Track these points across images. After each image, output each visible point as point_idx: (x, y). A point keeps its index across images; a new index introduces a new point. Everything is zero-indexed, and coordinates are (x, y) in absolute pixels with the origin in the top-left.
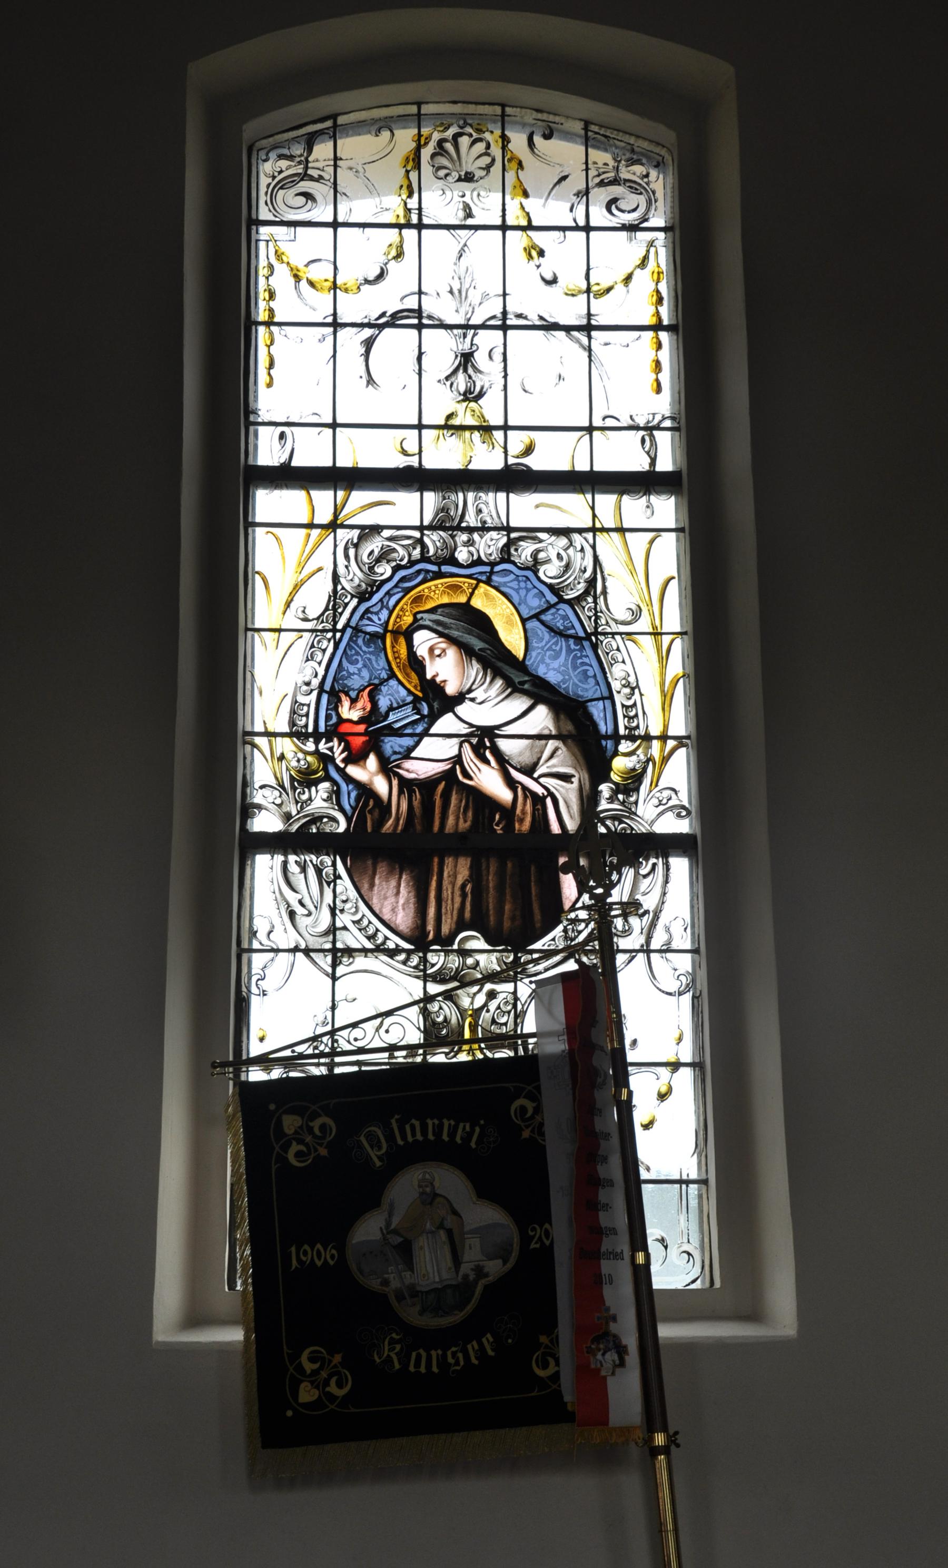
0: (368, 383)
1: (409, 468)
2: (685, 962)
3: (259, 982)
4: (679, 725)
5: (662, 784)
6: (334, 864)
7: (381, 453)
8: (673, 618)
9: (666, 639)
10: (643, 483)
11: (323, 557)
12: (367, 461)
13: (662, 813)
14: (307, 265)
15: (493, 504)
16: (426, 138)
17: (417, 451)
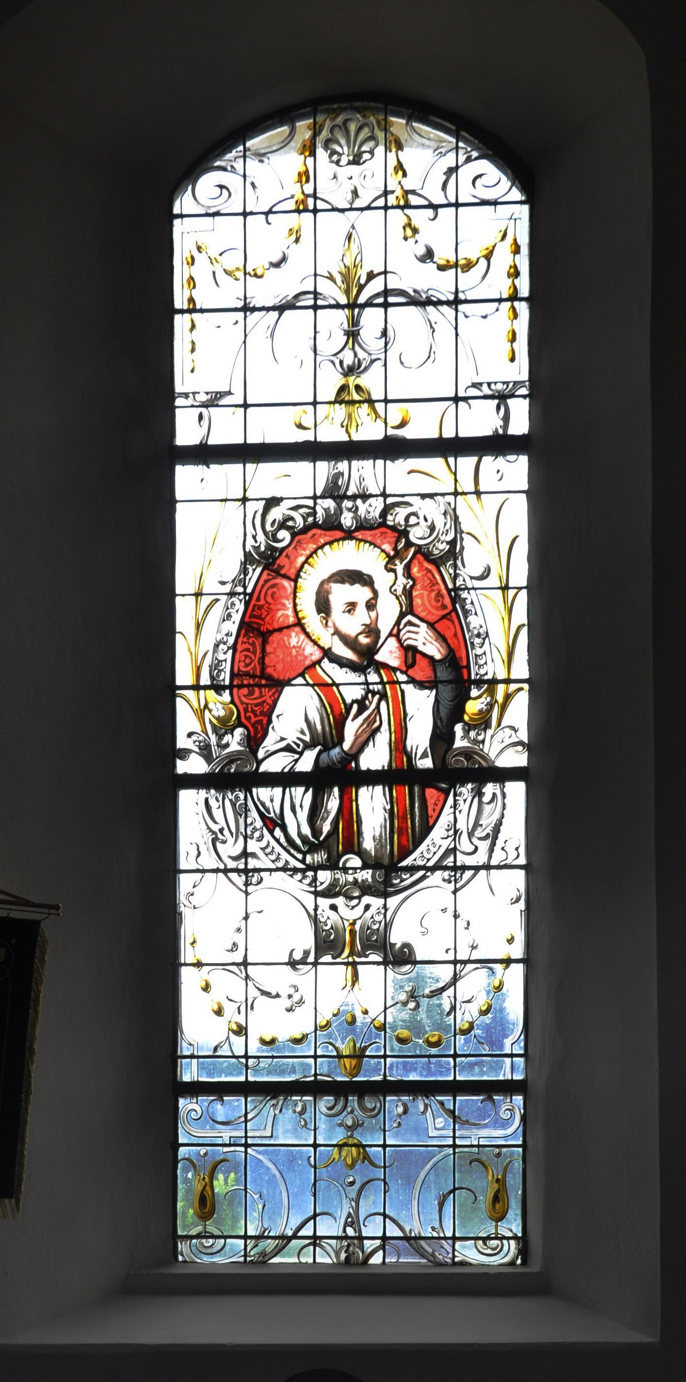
2: (518, 879)
4: (521, 669)
5: (503, 724)
7: (277, 428)
8: (520, 574)
9: (511, 593)
10: (499, 444)
14: (221, 255)
15: (365, 473)
16: (321, 126)
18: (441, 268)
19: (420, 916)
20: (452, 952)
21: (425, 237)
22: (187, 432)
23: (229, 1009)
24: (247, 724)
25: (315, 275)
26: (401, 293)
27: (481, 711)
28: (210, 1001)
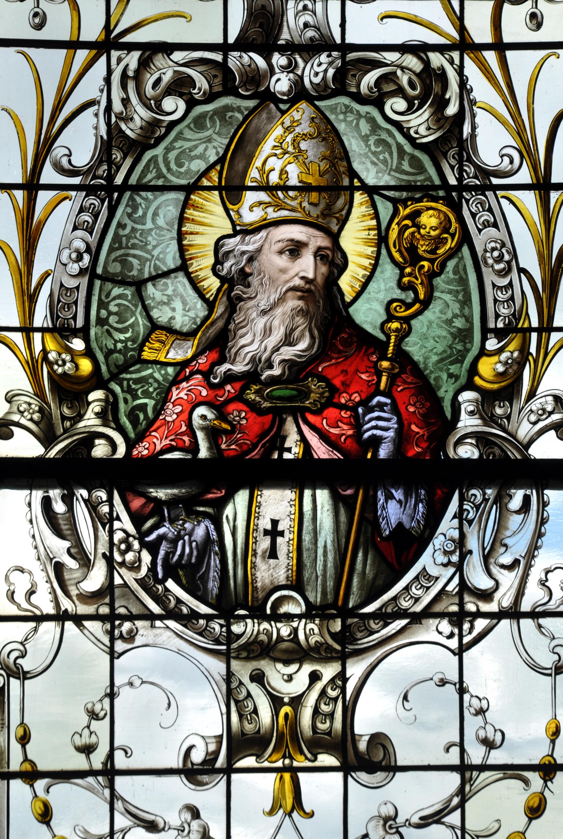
3: (19, 661)
11: (91, 87)
20: (455, 751)
24: (417, 153)
27: (501, 375)
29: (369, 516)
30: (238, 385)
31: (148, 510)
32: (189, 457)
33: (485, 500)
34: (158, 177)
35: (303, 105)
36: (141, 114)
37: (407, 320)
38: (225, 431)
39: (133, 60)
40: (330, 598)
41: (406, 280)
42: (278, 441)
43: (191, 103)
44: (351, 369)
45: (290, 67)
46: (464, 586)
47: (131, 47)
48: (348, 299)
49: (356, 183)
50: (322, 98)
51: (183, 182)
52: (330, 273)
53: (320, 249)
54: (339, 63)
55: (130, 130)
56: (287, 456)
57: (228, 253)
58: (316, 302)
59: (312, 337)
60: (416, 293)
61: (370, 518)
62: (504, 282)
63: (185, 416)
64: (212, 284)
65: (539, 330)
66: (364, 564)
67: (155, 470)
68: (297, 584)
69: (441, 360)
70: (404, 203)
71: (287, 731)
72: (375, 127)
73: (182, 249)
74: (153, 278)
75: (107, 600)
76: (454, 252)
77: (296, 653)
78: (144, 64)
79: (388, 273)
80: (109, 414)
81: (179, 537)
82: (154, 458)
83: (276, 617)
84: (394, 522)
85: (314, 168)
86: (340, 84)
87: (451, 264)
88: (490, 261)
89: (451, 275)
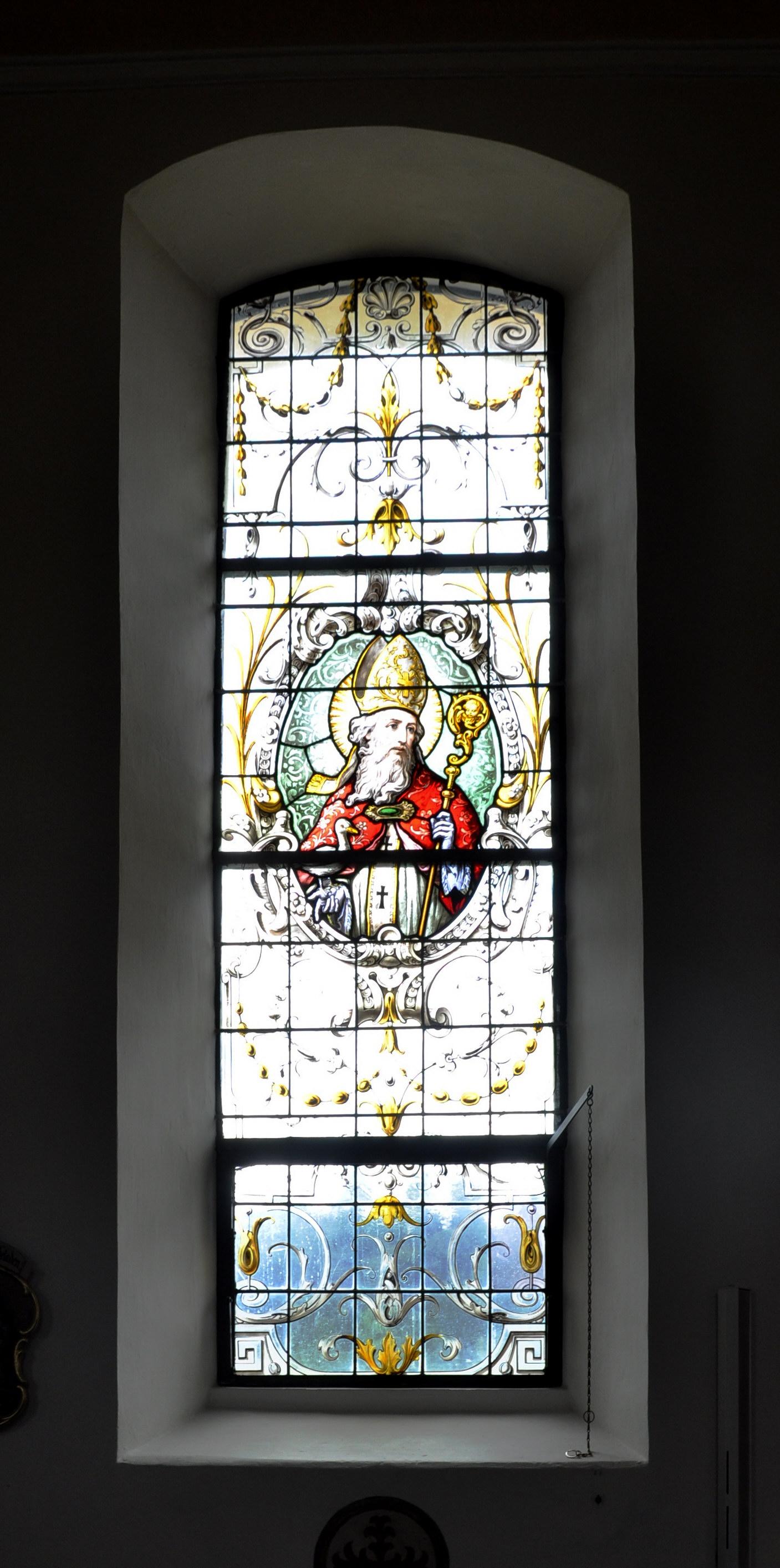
0: (318, 488)
1: (348, 558)
6: (288, 876)
10: (356, 1132)
11: (281, 631)
12: (316, 553)
13: (535, 832)
17: (354, 541)
18: (473, 407)
19: (455, 980)
21: (458, 382)
22: (236, 545)
23: (273, 1074)
24: (464, 666)
25: (356, 412)
26: (438, 428)
28: (255, 1066)
29: (437, 883)
30: (363, 806)
31: (310, 881)
32: (334, 849)
33: (504, 873)
34: (318, 682)
35: (399, 638)
36: (308, 646)
37: (459, 766)
38: (355, 834)
39: (303, 613)
40: (415, 931)
41: (458, 742)
42: (385, 840)
43: (337, 638)
44: (427, 796)
45: (392, 615)
46: (491, 924)
47: (302, 606)
48: (425, 754)
49: (430, 684)
50: (410, 633)
51: (331, 686)
52: (415, 738)
53: (409, 724)
54: (419, 612)
55: (303, 655)
56: (390, 848)
57: (356, 728)
58: (407, 756)
59: (405, 777)
60: (464, 749)
61: (438, 885)
62: (513, 743)
63: (332, 825)
64: (347, 747)
65: (534, 771)
66: (435, 911)
67: (315, 858)
68: (396, 924)
69: (478, 790)
70: (457, 695)
71: (390, 1007)
72: (440, 650)
73: (330, 726)
74: (313, 744)
75: (287, 933)
76: (485, 726)
77: (396, 963)
78: (310, 616)
79: (448, 738)
80: (289, 824)
81: (328, 897)
82: (313, 852)
83: (383, 942)
84: (451, 888)
85: (406, 676)
86: (420, 626)
87: (484, 732)
88: (506, 730)
89: (484, 739)
